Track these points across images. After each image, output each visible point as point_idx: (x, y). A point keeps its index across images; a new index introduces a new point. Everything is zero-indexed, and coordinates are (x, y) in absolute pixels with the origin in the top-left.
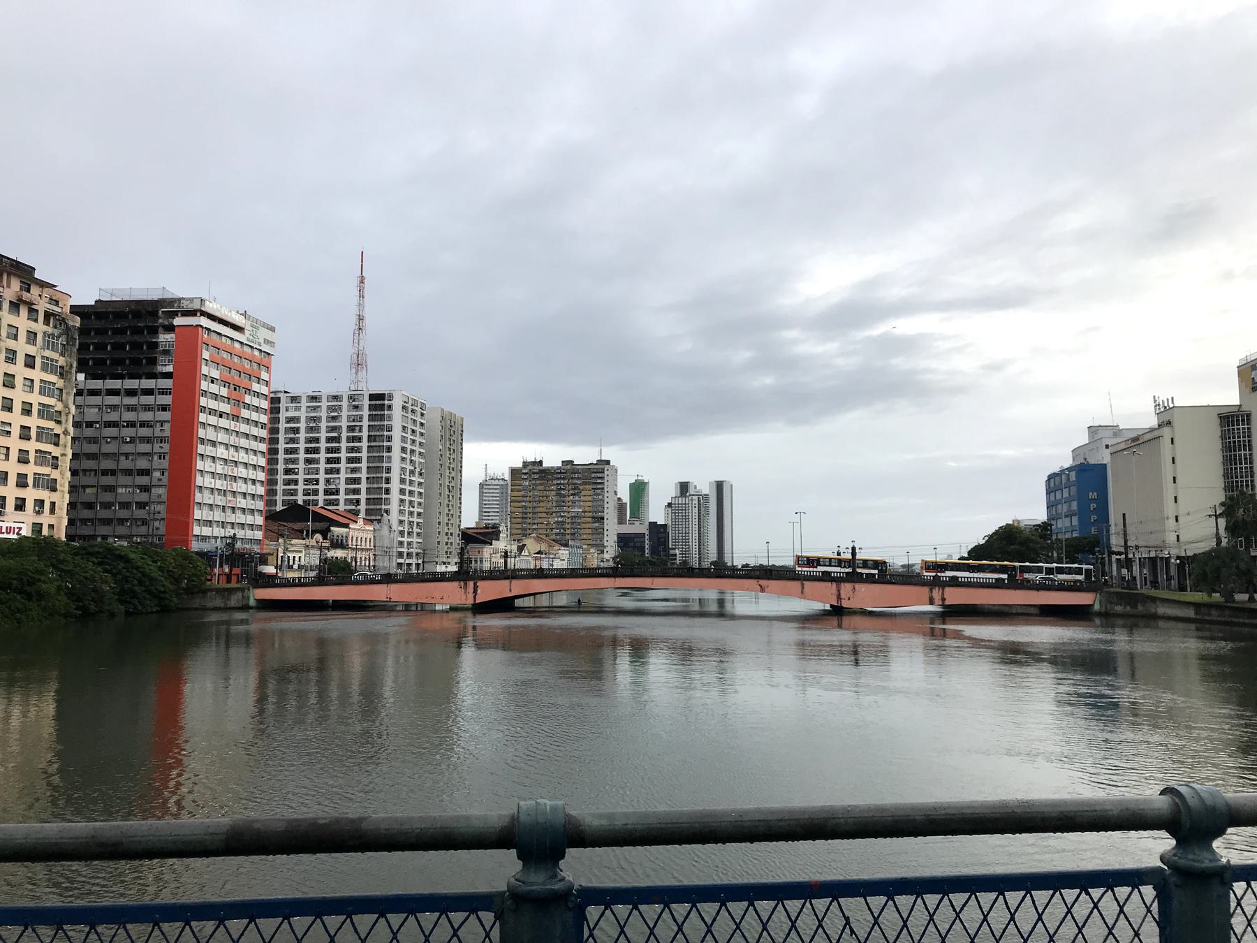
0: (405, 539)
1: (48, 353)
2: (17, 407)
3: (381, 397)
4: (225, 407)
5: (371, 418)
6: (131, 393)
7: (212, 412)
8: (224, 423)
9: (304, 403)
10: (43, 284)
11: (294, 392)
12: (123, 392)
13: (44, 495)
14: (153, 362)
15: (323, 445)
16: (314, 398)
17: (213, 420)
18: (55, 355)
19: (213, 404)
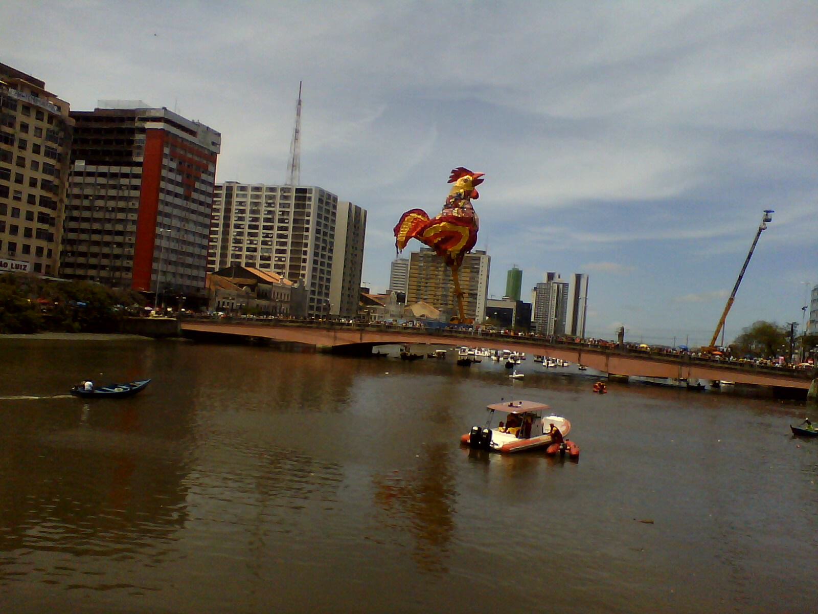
0: (316, 297)
1: (49, 144)
2: (26, 181)
3: (304, 191)
4: (180, 190)
5: (297, 206)
6: (114, 176)
7: (169, 193)
8: (178, 201)
9: (250, 192)
10: (49, 95)
11: (243, 182)
12: (84, 174)
13: (43, 244)
14: (130, 154)
15: (262, 223)
16: (257, 189)
17: (169, 199)
18: (55, 146)
19: (171, 187)
